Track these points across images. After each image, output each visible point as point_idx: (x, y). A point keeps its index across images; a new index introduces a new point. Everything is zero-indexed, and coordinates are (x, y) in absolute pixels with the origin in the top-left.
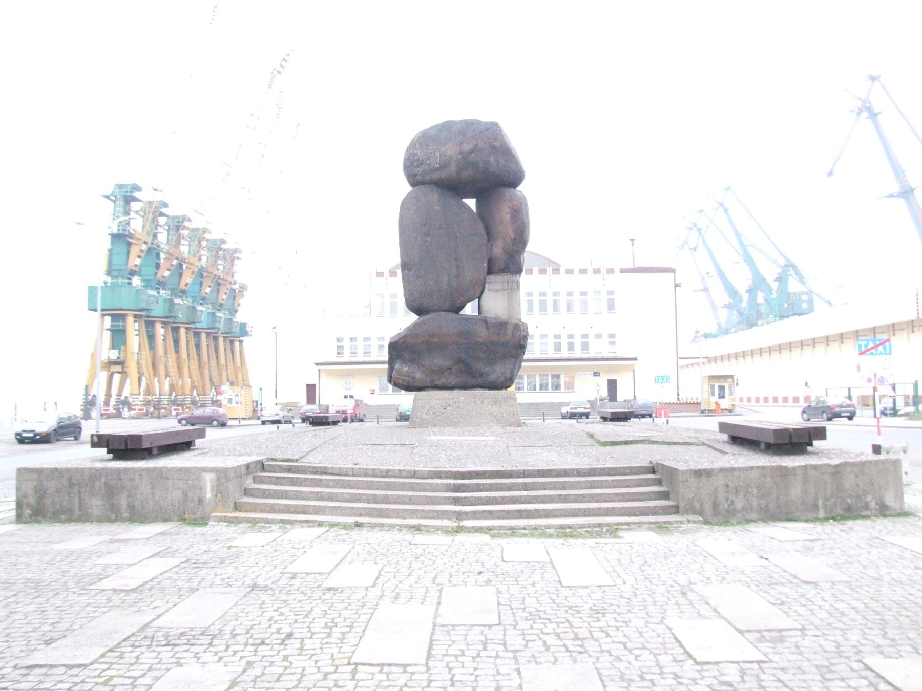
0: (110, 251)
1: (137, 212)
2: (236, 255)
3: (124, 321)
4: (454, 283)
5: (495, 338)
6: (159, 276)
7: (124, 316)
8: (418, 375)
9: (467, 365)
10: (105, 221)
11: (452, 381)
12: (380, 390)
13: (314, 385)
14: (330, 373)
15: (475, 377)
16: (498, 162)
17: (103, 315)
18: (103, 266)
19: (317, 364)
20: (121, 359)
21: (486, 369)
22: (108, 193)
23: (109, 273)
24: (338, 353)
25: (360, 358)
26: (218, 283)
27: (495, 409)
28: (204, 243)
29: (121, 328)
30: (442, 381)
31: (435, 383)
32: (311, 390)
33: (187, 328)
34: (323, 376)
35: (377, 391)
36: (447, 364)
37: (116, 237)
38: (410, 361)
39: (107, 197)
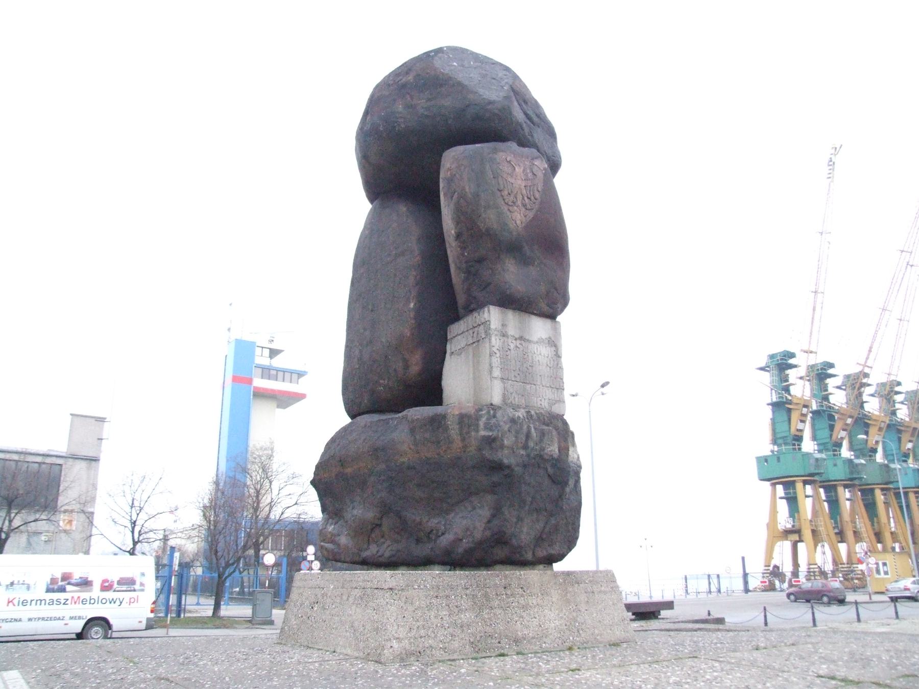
0: (773, 420)
1: (902, 403)
3: (794, 488)
5: (428, 452)
6: (834, 437)
7: (794, 482)
10: (763, 391)
11: (386, 549)
15: (418, 541)
17: (804, 485)
18: (767, 435)
20: (797, 527)
21: (433, 522)
22: (763, 365)
23: (774, 441)
28: (899, 398)
29: (871, 501)
36: (371, 515)
37: (776, 406)
39: (762, 369)
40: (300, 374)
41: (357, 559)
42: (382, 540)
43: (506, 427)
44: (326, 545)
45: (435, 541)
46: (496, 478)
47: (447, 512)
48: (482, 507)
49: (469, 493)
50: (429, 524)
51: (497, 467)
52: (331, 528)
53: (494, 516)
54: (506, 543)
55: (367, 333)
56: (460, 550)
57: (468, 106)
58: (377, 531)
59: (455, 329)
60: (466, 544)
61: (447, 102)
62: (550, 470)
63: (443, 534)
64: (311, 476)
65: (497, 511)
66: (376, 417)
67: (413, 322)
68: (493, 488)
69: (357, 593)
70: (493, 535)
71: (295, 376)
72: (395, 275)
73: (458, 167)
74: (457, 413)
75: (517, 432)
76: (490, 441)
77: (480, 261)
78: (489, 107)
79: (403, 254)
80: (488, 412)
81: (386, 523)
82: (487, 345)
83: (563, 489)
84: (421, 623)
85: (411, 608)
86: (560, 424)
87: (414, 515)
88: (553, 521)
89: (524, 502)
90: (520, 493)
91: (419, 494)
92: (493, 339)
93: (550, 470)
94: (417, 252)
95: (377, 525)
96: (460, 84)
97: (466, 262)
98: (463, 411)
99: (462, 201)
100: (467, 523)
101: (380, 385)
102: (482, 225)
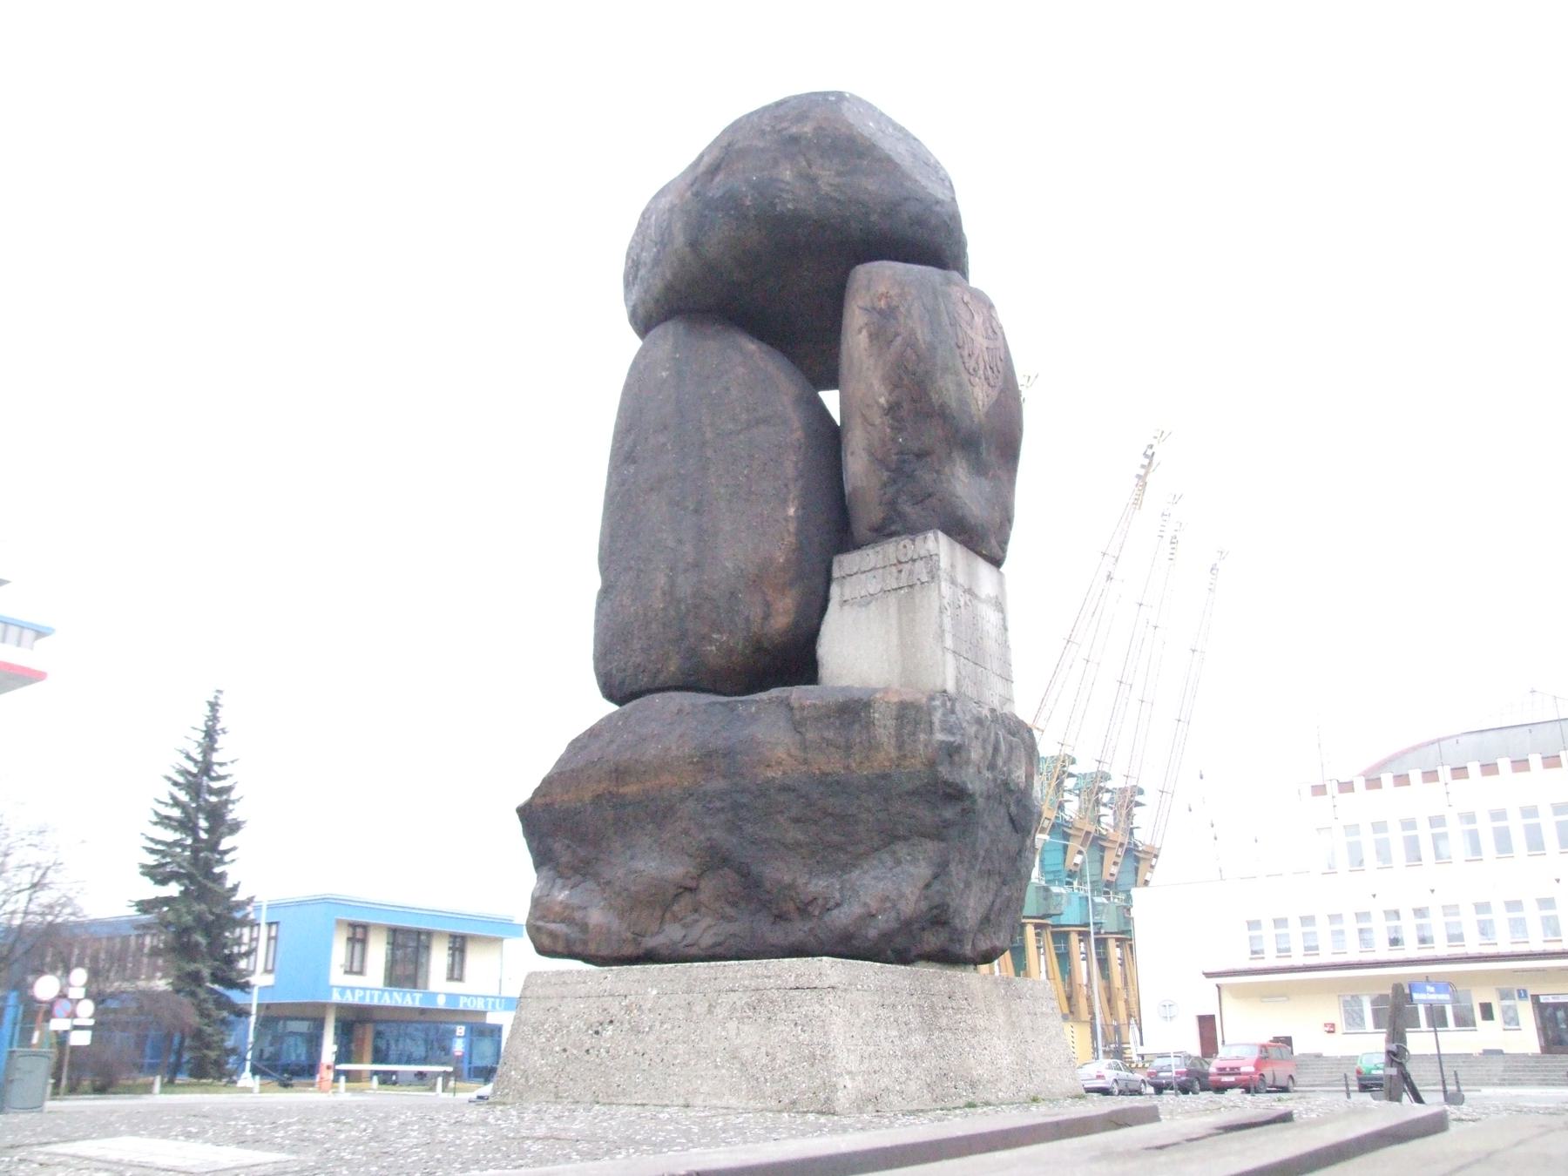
2: (1138, 798)
4: (685, 585)
5: (832, 763)
8: (596, 916)
9: (744, 873)
11: (705, 931)
12: (1348, 1024)
13: (1213, 1017)
14: (1242, 993)
15: (780, 917)
16: (813, 180)
19: (1208, 975)
21: (817, 885)
24: (1254, 952)
25: (1298, 959)
26: (1097, 843)
27: (747, 1036)
28: (1069, 783)
30: (673, 933)
31: (650, 942)
32: (1207, 1025)
33: (1037, 926)
34: (1227, 1000)
35: (1341, 1026)
36: (678, 870)
38: (576, 870)
40: (40, 633)
41: (628, 950)
42: (696, 916)
43: (972, 730)
44: (552, 926)
45: (820, 917)
46: (949, 813)
47: (845, 868)
48: (914, 861)
49: (890, 837)
50: (811, 888)
51: (956, 794)
52: (562, 896)
53: (936, 877)
54: (944, 924)
55: (687, 548)
56: (872, 933)
57: (906, 199)
58: (687, 899)
59: (846, 563)
60: (884, 922)
61: (871, 185)
62: (1013, 809)
63: (838, 905)
64: (525, 796)
65: (941, 870)
66: (704, 699)
67: (792, 539)
68: (938, 833)
69: (740, 999)
70: (931, 909)
71: (28, 635)
72: (751, 457)
73: (902, 295)
74: (895, 699)
75: (984, 741)
76: (952, 752)
77: (921, 455)
78: (938, 208)
79: (765, 421)
80: (944, 704)
81: (708, 888)
82: (935, 595)
83: (1024, 841)
84: (871, 1049)
85: (859, 1022)
86: (1026, 735)
87: (780, 872)
88: (1006, 892)
89: (976, 857)
90: (974, 844)
91: (795, 834)
92: (943, 584)
93: (1013, 809)
94: (796, 424)
95: (686, 889)
96: (889, 160)
97: (901, 453)
98: (908, 698)
99: (909, 351)
100: (887, 886)
101: (711, 642)
102: (934, 397)
